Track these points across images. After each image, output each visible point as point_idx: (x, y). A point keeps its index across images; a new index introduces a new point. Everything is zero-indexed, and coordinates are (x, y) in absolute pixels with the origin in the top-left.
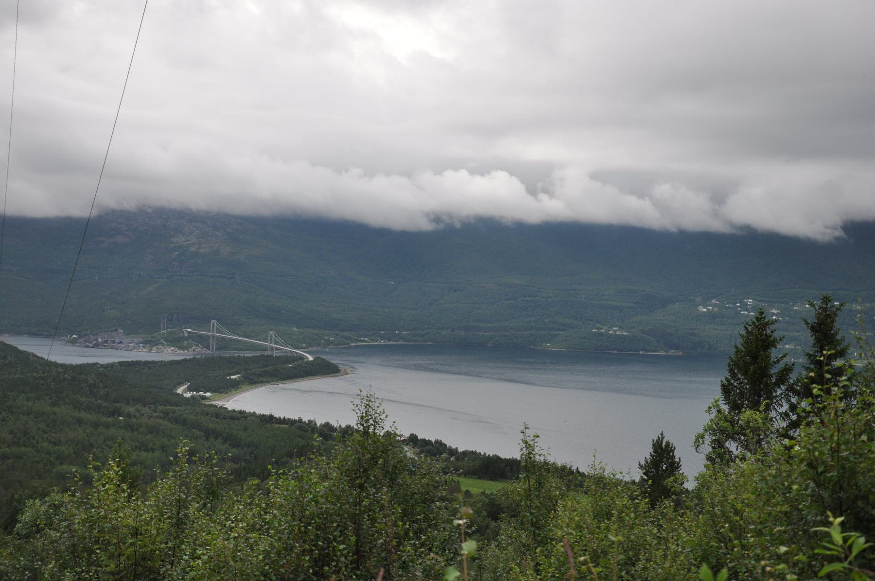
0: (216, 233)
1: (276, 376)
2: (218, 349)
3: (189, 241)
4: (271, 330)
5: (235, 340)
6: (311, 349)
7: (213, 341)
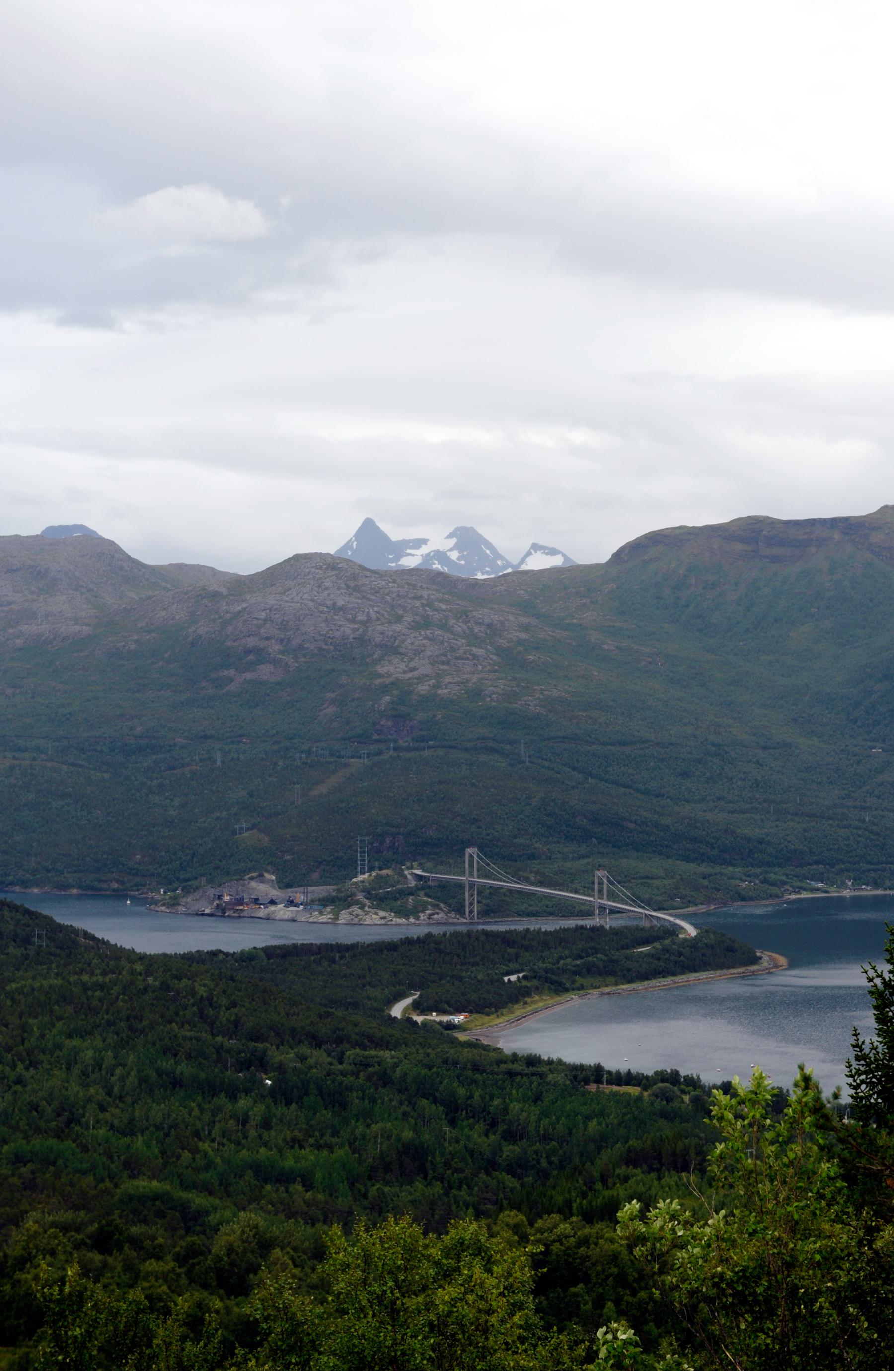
0: (474, 650)
1: (612, 973)
2: (484, 913)
3: (415, 669)
4: (600, 867)
5: (521, 893)
6: (691, 909)
7: (472, 895)
